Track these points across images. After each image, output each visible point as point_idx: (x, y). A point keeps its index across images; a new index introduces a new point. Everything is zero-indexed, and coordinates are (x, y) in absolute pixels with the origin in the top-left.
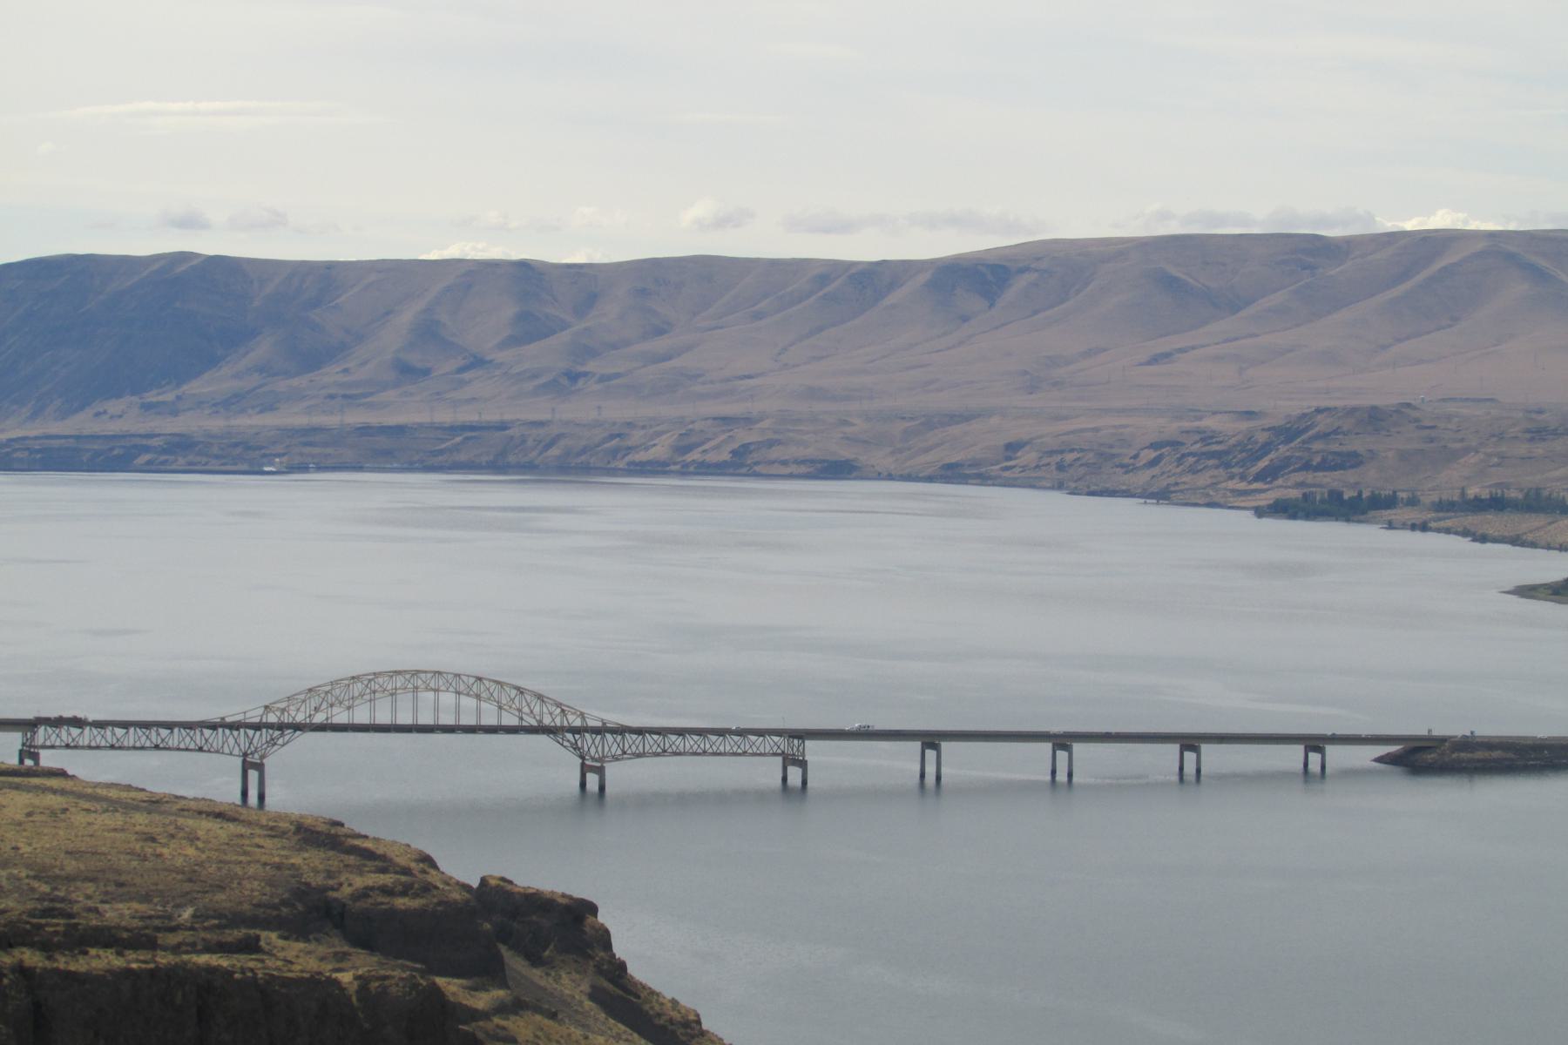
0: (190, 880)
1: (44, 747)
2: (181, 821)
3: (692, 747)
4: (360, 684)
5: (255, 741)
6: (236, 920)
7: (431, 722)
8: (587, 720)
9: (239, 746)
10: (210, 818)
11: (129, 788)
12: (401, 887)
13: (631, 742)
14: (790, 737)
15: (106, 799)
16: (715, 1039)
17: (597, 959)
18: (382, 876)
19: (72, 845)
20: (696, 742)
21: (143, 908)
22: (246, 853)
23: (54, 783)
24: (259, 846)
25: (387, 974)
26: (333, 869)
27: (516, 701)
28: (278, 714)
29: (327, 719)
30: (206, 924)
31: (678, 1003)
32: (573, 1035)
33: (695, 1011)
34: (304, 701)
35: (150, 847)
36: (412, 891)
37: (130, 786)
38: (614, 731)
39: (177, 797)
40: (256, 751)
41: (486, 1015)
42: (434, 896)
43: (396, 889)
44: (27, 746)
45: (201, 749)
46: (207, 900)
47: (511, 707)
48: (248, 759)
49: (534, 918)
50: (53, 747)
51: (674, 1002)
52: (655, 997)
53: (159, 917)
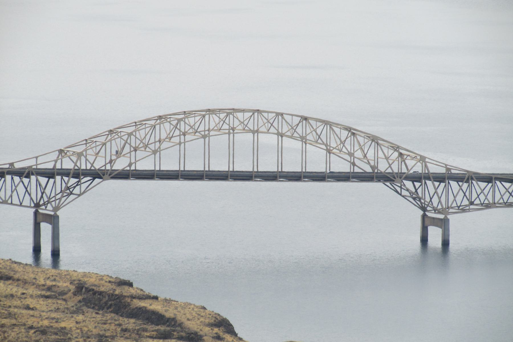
3: (502, 197)
4: (167, 125)
5: (48, 191)
7: (298, 169)
9: (30, 195)
13: (479, 191)
22: (10, 315)
24: (28, 308)
27: (347, 144)
28: (74, 158)
29: (130, 165)
34: (104, 144)
38: (459, 179)
47: (341, 151)
48: (40, 211)
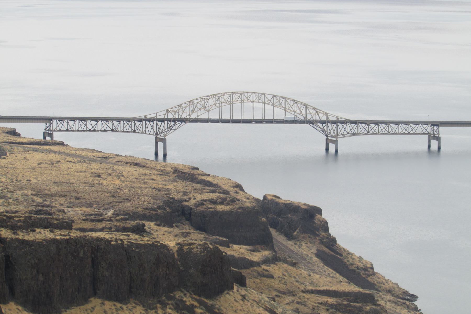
0: (113, 196)
1: (56, 130)
2: (116, 167)
3: (382, 130)
5: (161, 128)
6: (135, 216)
8: (329, 116)
9: (153, 130)
10: (132, 166)
11: (93, 151)
12: (220, 200)
13: (351, 128)
14: (432, 125)
15: (81, 156)
16: (380, 276)
17: (321, 236)
18: (211, 194)
19: (58, 179)
20: (384, 128)
21: (88, 210)
23: (56, 148)
24: (152, 179)
25: (192, 242)
26: (188, 191)
27: (293, 107)
28: (173, 113)
29: (198, 116)
30: (117, 218)
31: (362, 258)
32: (303, 274)
33: (370, 262)
35: (97, 180)
36: (226, 202)
37: (94, 150)
38: (342, 122)
39: (117, 155)
40: (162, 133)
41: (258, 264)
42: (237, 204)
43: (218, 201)
44: (47, 130)
45: (134, 132)
46: (121, 206)
49: (289, 215)
50: (60, 131)
51: (360, 258)
52: (350, 255)
53: (96, 215)
